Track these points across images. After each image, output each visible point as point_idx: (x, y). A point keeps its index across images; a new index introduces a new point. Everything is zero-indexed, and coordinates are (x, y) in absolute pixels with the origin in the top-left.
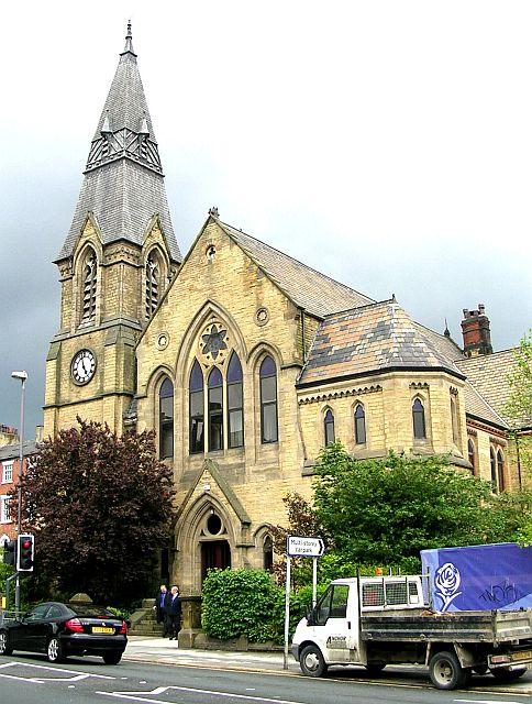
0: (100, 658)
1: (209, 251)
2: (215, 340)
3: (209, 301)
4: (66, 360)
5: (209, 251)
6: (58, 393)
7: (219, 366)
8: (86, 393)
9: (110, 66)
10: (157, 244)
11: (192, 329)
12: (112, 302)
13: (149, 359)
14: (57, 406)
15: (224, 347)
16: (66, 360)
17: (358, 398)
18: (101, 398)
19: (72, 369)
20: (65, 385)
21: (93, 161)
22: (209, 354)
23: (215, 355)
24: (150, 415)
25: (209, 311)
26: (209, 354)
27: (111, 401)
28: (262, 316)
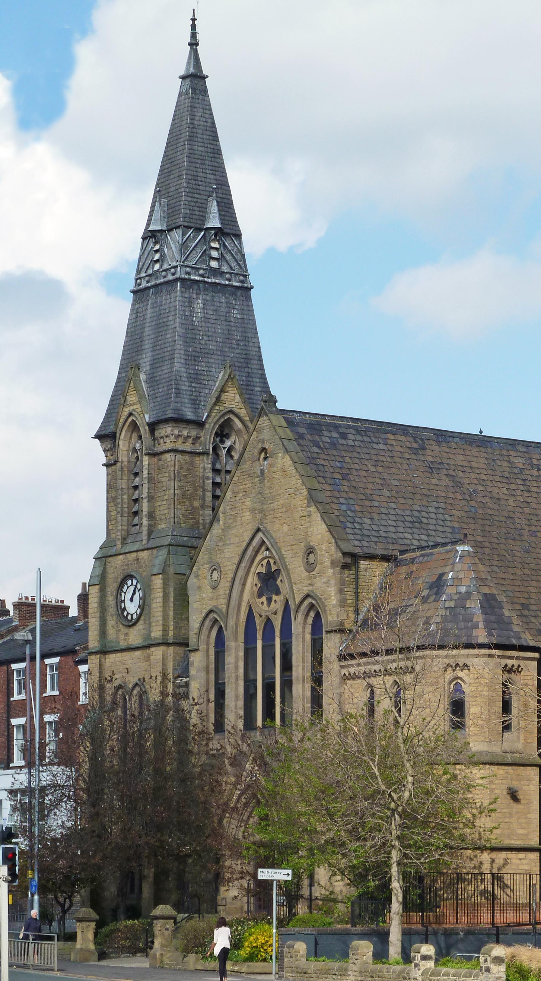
0: (11, 903)
1: (263, 455)
2: (269, 581)
3: (258, 530)
4: (111, 588)
5: (263, 455)
6: (103, 633)
7: (272, 617)
8: (135, 637)
9: (171, 90)
10: (231, 412)
11: (243, 564)
12: (164, 509)
13: (202, 598)
14: (103, 652)
15: (278, 593)
16: (111, 588)
17: (460, 674)
18: (148, 647)
19: (119, 602)
20: (111, 622)
21: (143, 275)
22: (264, 599)
23: (269, 600)
24: (203, 674)
25: (259, 542)
26: (264, 599)
27: (157, 653)
28: (312, 558)
